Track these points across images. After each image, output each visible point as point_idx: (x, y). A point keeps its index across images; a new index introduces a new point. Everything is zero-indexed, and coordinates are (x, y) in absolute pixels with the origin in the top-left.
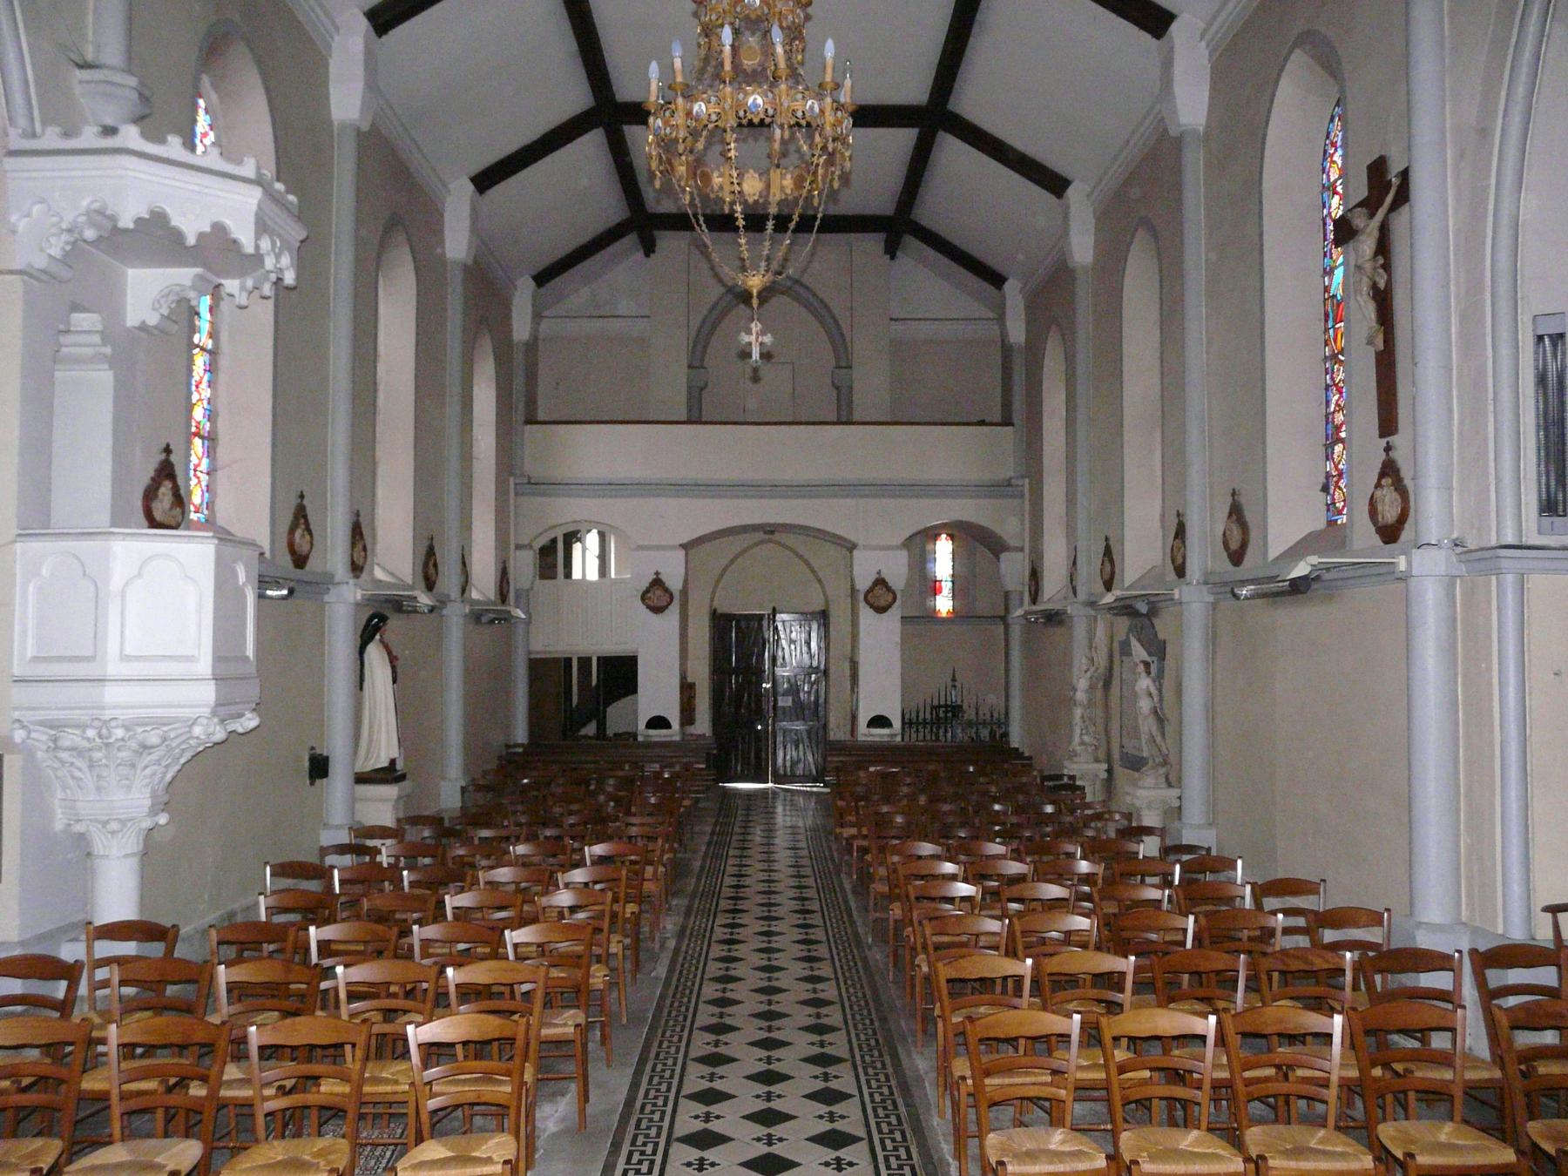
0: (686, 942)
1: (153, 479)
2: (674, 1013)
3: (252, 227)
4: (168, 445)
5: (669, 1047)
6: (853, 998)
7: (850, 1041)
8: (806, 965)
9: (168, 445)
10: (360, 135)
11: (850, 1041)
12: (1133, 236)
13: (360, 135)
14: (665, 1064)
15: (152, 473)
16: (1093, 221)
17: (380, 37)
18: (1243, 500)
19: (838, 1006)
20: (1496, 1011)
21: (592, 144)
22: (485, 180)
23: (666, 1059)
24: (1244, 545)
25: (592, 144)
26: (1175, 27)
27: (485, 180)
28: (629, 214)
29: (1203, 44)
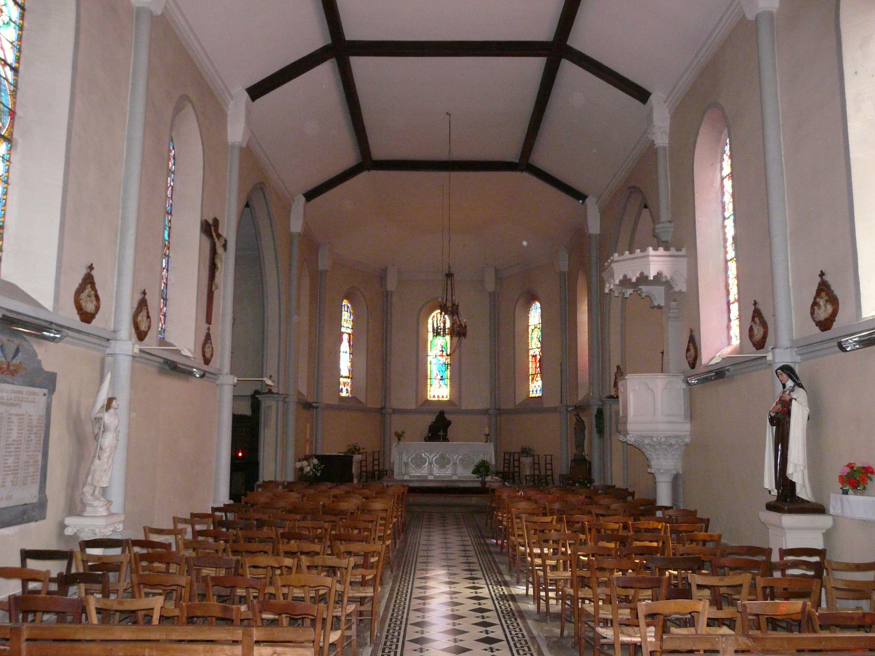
0: (398, 584)
1: (80, 285)
2: (389, 643)
3: (643, 647)
4: (92, 265)
5: (394, 632)
6: (516, 639)
7: (504, 630)
8: (483, 629)
9: (92, 265)
10: (241, 149)
11: (504, 630)
12: (578, 274)
13: (241, 149)
14: (392, 642)
15: (80, 281)
16: (599, 215)
17: (303, 195)
18: (760, 307)
19: (505, 643)
20: (276, 382)
21: (326, 71)
22: (257, 91)
23: (392, 639)
24: (764, 337)
25: (326, 71)
26: (651, 98)
27: (257, 91)
28: (330, 42)
29: (666, 105)
